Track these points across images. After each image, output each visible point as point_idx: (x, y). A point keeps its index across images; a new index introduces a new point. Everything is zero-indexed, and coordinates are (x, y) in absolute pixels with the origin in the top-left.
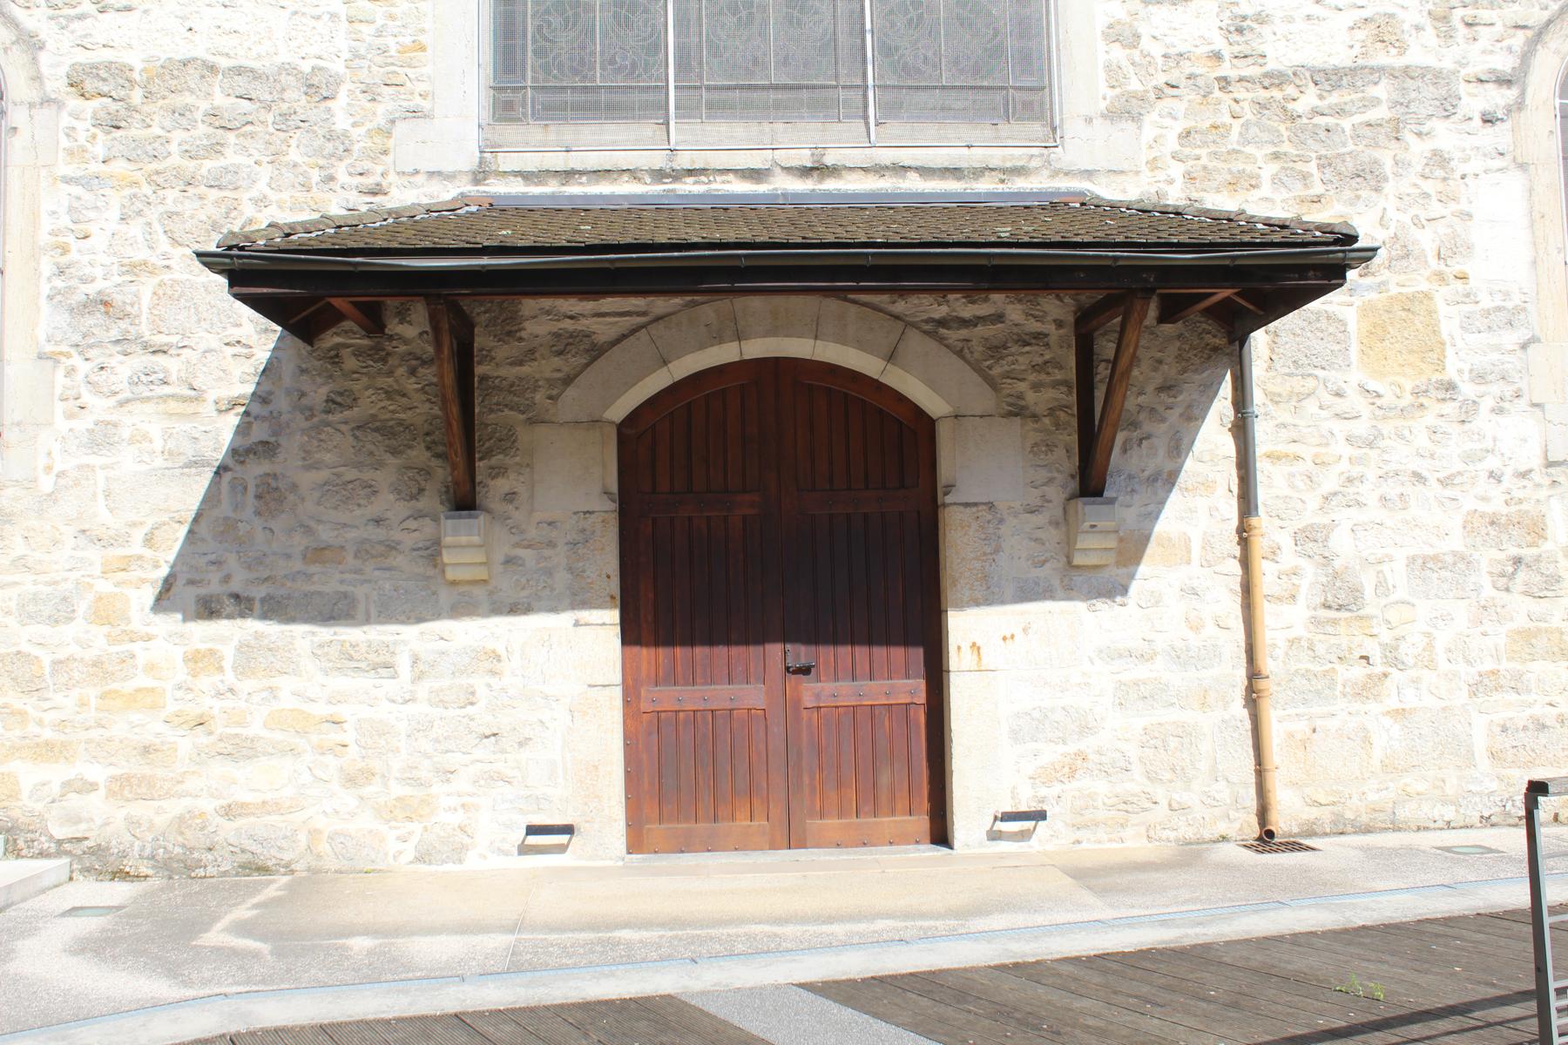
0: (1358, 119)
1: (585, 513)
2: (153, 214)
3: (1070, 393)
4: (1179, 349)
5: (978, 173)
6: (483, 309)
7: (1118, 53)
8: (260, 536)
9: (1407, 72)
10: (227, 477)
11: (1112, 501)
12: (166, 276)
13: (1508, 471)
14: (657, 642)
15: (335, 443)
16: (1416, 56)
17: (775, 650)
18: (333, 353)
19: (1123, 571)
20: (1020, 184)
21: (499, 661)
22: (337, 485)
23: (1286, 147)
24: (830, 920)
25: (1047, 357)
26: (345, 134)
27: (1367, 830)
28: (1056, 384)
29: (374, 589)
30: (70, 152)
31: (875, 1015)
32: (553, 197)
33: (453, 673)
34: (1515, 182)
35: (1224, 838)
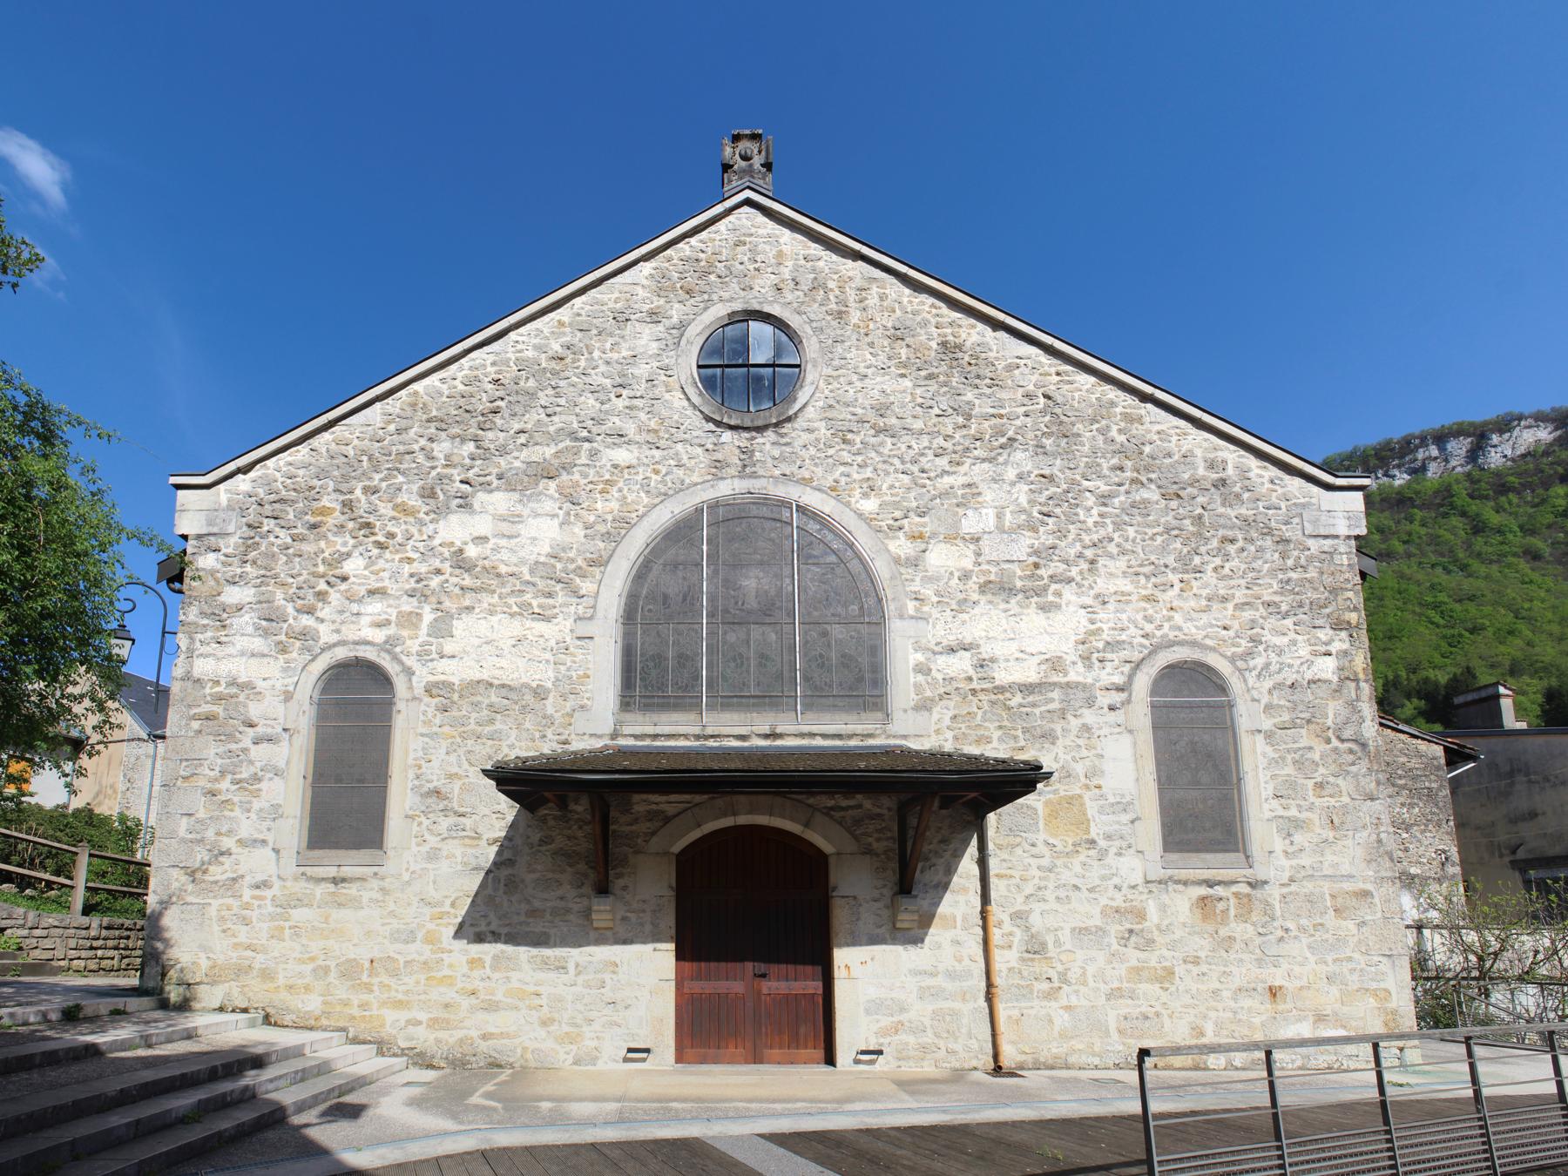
0: (1043, 708)
2: (461, 751)
5: (850, 736)
7: (920, 678)
8: (506, 904)
9: (1068, 684)
10: (491, 875)
11: (916, 897)
12: (467, 780)
13: (1125, 885)
16: (1073, 677)
17: (749, 965)
20: (871, 742)
23: (1005, 723)
24: (774, 1101)
26: (552, 716)
27: (1052, 1068)
28: (888, 839)
30: (424, 722)
31: (795, 1153)
32: (648, 747)
34: (1126, 740)
35: (975, 1069)
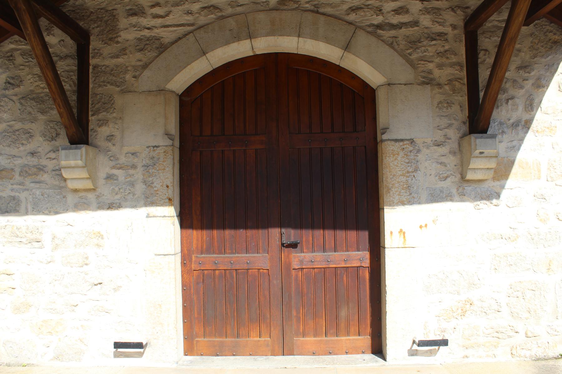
1: (154, 147)
3: (462, 70)
4: (532, 42)
6: (96, 25)
11: (494, 136)
14: (202, 227)
15: (9, 107)
17: (275, 232)
18: (9, 54)
19: (497, 183)
21: (102, 238)
22: (10, 132)
25: (447, 48)
28: (452, 65)
29: (30, 194)
33: (75, 246)
